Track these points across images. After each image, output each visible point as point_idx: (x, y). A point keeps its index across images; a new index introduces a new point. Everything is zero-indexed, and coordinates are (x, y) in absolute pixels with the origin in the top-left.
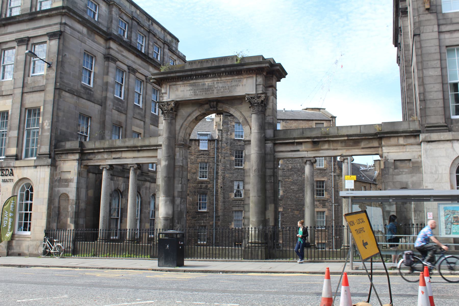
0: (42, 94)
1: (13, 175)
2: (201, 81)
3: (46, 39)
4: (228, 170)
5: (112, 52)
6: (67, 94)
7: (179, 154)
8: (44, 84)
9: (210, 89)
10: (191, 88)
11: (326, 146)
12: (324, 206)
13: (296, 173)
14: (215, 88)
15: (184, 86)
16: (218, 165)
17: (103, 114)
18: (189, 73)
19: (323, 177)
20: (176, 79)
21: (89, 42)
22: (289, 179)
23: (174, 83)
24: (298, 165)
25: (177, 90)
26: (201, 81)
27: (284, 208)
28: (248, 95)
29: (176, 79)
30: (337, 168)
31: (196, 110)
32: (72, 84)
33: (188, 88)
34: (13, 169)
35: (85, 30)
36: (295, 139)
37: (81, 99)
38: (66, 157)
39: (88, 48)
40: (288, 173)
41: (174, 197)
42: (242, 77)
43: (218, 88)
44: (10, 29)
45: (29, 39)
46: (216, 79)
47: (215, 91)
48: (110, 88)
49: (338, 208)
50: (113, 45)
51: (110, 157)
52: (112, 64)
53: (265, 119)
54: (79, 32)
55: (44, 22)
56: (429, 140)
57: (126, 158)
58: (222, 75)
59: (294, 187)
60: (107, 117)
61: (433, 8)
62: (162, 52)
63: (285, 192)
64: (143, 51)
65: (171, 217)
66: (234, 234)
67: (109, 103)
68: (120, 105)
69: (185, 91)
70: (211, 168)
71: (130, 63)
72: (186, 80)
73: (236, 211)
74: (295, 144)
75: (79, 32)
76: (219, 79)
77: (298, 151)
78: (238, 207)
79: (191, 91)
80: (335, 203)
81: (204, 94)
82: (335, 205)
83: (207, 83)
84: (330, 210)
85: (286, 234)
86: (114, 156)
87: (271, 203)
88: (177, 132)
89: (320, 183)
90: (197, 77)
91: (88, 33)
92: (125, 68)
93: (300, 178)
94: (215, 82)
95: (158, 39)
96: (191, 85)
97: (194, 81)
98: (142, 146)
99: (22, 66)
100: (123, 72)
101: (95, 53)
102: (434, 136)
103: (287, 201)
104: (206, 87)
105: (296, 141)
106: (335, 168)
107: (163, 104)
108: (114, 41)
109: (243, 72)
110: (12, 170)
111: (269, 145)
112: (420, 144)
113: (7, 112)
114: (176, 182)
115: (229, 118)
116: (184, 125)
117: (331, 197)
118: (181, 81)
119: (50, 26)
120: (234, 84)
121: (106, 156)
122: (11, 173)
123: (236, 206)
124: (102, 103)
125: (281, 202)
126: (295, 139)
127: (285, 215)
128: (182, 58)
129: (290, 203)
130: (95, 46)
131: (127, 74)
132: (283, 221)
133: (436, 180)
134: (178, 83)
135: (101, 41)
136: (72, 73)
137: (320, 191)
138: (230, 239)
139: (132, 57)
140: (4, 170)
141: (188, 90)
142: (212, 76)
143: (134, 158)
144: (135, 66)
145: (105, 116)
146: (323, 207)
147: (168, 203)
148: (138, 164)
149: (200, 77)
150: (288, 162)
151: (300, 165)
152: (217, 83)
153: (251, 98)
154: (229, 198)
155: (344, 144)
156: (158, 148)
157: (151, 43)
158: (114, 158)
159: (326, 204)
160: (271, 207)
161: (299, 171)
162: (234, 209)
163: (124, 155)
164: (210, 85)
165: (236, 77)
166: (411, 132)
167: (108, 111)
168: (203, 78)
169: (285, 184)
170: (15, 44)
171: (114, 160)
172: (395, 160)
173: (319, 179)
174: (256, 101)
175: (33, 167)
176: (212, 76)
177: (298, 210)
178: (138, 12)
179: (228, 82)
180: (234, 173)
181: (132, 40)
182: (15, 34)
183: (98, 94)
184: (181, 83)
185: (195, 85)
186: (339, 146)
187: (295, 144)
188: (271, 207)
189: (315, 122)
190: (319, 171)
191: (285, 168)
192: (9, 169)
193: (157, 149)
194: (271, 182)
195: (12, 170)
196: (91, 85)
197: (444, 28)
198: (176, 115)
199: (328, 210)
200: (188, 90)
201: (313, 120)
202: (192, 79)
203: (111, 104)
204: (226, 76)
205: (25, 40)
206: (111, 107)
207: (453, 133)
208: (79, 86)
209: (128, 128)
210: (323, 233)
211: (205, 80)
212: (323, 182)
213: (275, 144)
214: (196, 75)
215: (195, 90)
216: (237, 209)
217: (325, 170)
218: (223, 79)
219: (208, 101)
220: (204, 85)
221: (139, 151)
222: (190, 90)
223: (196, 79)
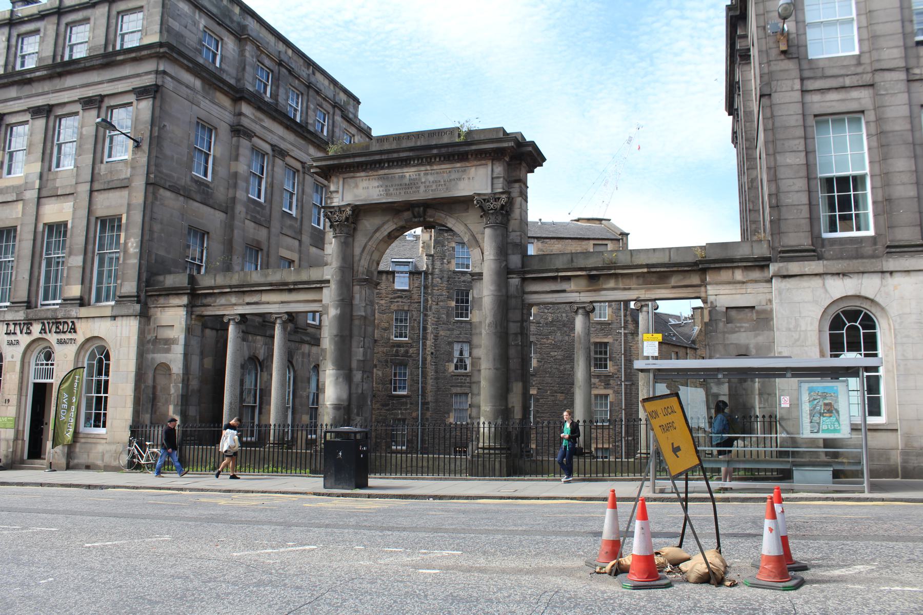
0: (125, 193)
1: (75, 332)
2: (398, 171)
3: (131, 98)
4: (443, 324)
5: (245, 122)
6: (168, 194)
7: (360, 296)
8: (128, 175)
9: (412, 184)
10: (381, 183)
11: (612, 284)
12: (607, 385)
13: (559, 329)
14: (422, 183)
15: (369, 180)
16: (426, 315)
17: (229, 227)
18: (377, 157)
19: (606, 336)
20: (354, 167)
21: (205, 104)
22: (548, 339)
23: (352, 174)
24: (564, 315)
25: (357, 186)
26: (397, 171)
27: (539, 389)
28: (479, 195)
29: (354, 167)
30: (630, 322)
31: (388, 221)
32: (175, 175)
33: (376, 183)
34: (75, 321)
35: (198, 84)
36: (558, 270)
37: (191, 202)
38: (166, 302)
39: (203, 114)
40: (546, 330)
41: (350, 370)
42: (467, 164)
43: (427, 184)
44: (70, 81)
45: (102, 98)
46: (423, 168)
47: (422, 189)
48: (241, 184)
49: (631, 390)
50: (246, 109)
51: (241, 301)
52: (244, 142)
53: (507, 236)
54: (187, 87)
55: (127, 70)
56: (785, 273)
57: (268, 303)
58: (433, 160)
59: (556, 353)
60: (236, 232)
61: (793, 50)
62: (331, 122)
63: (541, 362)
64: (298, 120)
65: (346, 404)
66: (453, 434)
67: (240, 209)
68: (258, 212)
69: (370, 187)
70: (415, 320)
71: (275, 140)
72: (372, 169)
73: (456, 394)
74: (559, 280)
75: (187, 87)
76: (428, 168)
77: (564, 291)
78: (461, 386)
79: (381, 189)
80: (625, 381)
81: (402, 194)
82: (627, 383)
83: (407, 175)
84: (617, 393)
85: (543, 433)
86: (248, 299)
87: (516, 380)
88: (356, 258)
89: (601, 347)
90: (391, 164)
91: (203, 89)
92: (267, 148)
93: (567, 338)
94: (422, 173)
95: (324, 99)
96: (381, 178)
97: (386, 171)
98: (295, 283)
99: (89, 146)
100: (263, 154)
101: (215, 122)
102: (794, 267)
103: (545, 377)
104: (406, 181)
105: (560, 274)
106: (626, 322)
107: (332, 210)
108: (249, 102)
109: (470, 156)
110: (73, 323)
111: (515, 281)
112: (770, 281)
113: (65, 224)
114: (354, 344)
115: (446, 235)
116: (368, 247)
117: (619, 371)
118: (363, 171)
119: (138, 75)
120: (454, 176)
121: (233, 300)
122: (71, 329)
123: (457, 386)
124: (228, 208)
125: (535, 379)
126: (558, 270)
127: (541, 400)
128: (365, 132)
129: (549, 380)
130: (215, 110)
131: (271, 158)
132: (538, 412)
133: (797, 340)
134: (358, 175)
135: (226, 102)
136: (175, 156)
137: (601, 359)
138: (447, 442)
139: (279, 130)
140: (60, 323)
141: (375, 187)
142: (416, 162)
143: (282, 302)
144: (283, 145)
145: (232, 231)
146: (605, 388)
147: (341, 380)
148: (289, 314)
149: (395, 164)
150: (546, 311)
151: (567, 316)
152: (425, 174)
153: (484, 200)
154: (445, 371)
155: (641, 281)
156: (323, 285)
157: (312, 106)
158: (248, 304)
159: (612, 382)
160: (517, 388)
161: (564, 325)
162: (454, 390)
163: (265, 298)
164: (412, 177)
165: (458, 165)
166: (756, 260)
167: (237, 223)
168: (401, 167)
169: (541, 349)
170: (78, 107)
171: (248, 307)
172: (727, 308)
173: (598, 340)
174: (492, 206)
175: (109, 319)
176: (416, 162)
177: (562, 393)
178: (290, 52)
179: (444, 172)
180: (453, 330)
181: (280, 100)
182: (78, 90)
183: (221, 194)
184: (363, 174)
185: (388, 178)
186: (633, 283)
187: (559, 280)
188: (517, 388)
189: (592, 242)
190: (599, 327)
191: (542, 321)
192: (69, 321)
193: (322, 288)
194: (517, 345)
195: (73, 323)
196: (209, 178)
197: (810, 85)
198: (355, 229)
199: (614, 392)
200: (375, 187)
201: (589, 239)
202: (383, 168)
203: (244, 210)
204: (441, 162)
205: (96, 100)
206: (243, 215)
207: (825, 262)
208: (188, 179)
209: (272, 252)
210: (606, 432)
211: (405, 170)
212: (606, 344)
213: (524, 280)
214: (388, 161)
215: (387, 186)
216: (459, 390)
217: (609, 324)
218: (435, 167)
219: (409, 206)
220: (403, 177)
221: (290, 290)
222: (378, 187)
223: (389, 167)
